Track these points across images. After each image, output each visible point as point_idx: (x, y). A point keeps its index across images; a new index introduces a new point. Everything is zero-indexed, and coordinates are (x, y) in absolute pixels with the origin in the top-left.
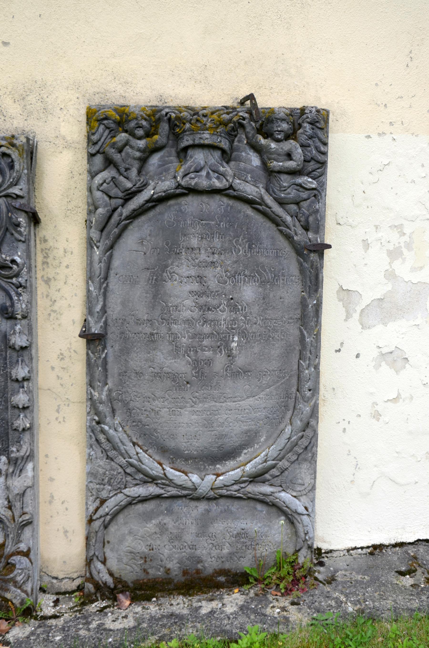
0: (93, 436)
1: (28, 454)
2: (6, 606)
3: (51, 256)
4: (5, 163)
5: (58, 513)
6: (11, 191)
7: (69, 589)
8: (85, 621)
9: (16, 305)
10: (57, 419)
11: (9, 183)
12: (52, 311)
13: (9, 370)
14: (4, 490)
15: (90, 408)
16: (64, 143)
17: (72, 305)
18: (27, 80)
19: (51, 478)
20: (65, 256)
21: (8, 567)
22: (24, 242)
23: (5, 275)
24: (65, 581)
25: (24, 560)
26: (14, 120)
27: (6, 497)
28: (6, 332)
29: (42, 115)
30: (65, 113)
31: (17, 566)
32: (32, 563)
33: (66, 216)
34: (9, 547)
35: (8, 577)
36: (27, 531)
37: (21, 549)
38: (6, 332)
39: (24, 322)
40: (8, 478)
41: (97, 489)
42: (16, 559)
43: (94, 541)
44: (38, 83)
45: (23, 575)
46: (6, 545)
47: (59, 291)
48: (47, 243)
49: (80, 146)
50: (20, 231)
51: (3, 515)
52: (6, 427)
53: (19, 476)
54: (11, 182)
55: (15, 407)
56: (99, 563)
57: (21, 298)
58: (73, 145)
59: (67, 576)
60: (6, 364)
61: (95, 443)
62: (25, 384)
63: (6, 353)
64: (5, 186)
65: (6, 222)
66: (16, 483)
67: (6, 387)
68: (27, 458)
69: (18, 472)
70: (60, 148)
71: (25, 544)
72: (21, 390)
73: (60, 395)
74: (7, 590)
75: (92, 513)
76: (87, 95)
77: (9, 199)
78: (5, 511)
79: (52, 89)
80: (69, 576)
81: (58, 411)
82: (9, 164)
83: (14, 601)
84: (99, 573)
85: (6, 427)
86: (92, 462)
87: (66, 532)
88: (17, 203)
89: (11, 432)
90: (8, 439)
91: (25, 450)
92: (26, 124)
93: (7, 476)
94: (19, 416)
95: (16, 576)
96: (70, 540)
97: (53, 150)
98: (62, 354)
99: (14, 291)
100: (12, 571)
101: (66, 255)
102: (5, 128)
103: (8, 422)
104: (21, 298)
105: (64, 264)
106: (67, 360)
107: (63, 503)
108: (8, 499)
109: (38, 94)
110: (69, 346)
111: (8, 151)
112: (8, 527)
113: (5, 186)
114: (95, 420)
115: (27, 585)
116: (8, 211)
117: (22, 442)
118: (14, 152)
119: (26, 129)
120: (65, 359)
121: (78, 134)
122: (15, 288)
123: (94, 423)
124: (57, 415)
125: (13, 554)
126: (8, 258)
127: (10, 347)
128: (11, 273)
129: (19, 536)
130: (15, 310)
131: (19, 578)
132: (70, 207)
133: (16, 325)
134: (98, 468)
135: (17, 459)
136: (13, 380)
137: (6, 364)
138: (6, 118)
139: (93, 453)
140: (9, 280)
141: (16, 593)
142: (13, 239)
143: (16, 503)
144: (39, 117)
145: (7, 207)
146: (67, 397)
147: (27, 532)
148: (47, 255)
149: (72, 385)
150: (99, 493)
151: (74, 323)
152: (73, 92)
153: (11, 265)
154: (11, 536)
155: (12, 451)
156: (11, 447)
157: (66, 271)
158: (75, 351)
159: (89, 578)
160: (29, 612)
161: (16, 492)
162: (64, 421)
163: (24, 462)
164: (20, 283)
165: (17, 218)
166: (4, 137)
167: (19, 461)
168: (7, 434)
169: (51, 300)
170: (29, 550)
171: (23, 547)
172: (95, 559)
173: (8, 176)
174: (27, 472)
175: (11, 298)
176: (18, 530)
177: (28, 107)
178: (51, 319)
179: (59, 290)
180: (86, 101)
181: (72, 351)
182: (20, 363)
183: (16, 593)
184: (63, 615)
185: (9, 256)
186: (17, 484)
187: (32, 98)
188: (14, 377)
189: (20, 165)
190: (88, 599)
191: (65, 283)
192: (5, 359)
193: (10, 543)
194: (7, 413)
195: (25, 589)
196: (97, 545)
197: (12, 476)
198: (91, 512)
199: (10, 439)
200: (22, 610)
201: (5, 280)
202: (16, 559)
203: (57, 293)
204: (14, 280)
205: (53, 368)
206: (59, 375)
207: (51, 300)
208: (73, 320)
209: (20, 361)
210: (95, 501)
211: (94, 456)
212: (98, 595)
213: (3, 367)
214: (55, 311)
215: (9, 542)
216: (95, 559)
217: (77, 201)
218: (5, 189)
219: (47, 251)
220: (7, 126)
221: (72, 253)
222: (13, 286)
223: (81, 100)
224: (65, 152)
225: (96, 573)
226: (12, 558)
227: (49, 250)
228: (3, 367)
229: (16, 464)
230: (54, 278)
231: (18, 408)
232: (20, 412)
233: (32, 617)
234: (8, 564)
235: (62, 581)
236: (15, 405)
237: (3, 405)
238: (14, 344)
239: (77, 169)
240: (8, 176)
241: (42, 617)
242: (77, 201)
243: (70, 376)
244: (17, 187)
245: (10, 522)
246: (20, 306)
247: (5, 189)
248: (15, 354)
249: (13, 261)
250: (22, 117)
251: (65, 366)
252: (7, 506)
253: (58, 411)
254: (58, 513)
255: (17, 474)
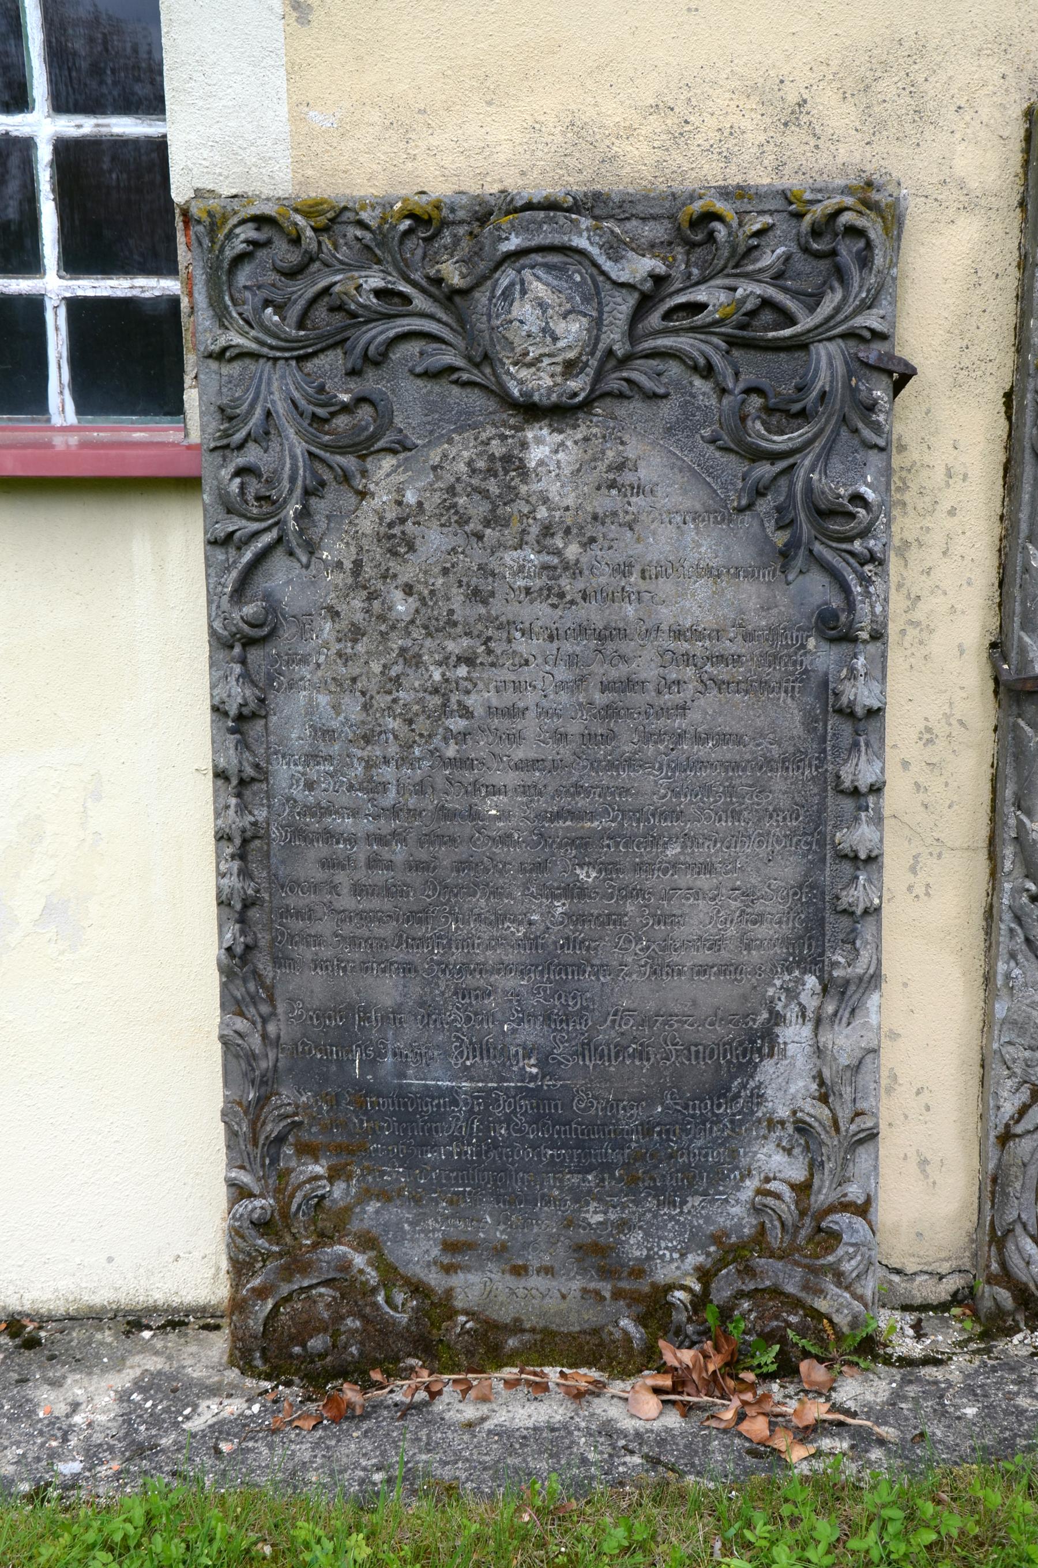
0: (1019, 931)
1: (871, 971)
2: (816, 1328)
3: (914, 487)
4: (850, 251)
5: (906, 1117)
6: (859, 321)
7: (933, 1299)
8: (1014, 1377)
9: (859, 606)
10: (910, 888)
11: (857, 303)
12: (911, 623)
13: (830, 767)
14: (810, 1057)
15: (1013, 863)
16: (962, 198)
17: (959, 607)
18: (878, 39)
19: (891, 1030)
20: (948, 485)
21: (817, 1238)
22: (882, 449)
23: (838, 532)
24: (919, 1279)
25: (859, 1222)
26: (840, 145)
27: (814, 1073)
28: (826, 674)
29: (909, 128)
30: (967, 118)
31: (845, 1238)
32: (874, 1233)
33: (957, 385)
34: (824, 1191)
35: (822, 1261)
36: (864, 1156)
37: (851, 1197)
38: (826, 674)
39: (871, 648)
40: (821, 1029)
41: (1025, 1060)
42: (841, 1220)
43: (1018, 1185)
44: (906, 45)
45: (859, 1258)
46: (815, 1187)
47: (928, 573)
48: (905, 454)
49: (1002, 203)
50: (878, 423)
51: (812, 1116)
52: (820, 905)
53: (849, 1024)
54: (863, 300)
55: (846, 856)
56: (1029, 1240)
57: (872, 589)
58: (983, 202)
59: (925, 1268)
60: (824, 751)
61: (1024, 947)
62: (871, 800)
63: (825, 725)
64: (848, 310)
65: (842, 401)
66: (841, 1041)
67: (822, 808)
68: (869, 982)
69: (847, 1015)
70: (951, 211)
71: (859, 1187)
72: (863, 814)
73: (919, 830)
74: (820, 1292)
75: (1012, 1118)
76: (1029, 66)
77: (852, 343)
78: (813, 1106)
79: (939, 59)
80: (930, 1269)
81: (913, 869)
82: (859, 253)
83: (836, 1319)
84: (1028, 1263)
85: (820, 905)
86: (1012, 995)
87: (924, 1163)
88: (872, 353)
89: (829, 917)
90: (824, 935)
91: (866, 961)
92: (868, 155)
93: (818, 1022)
94: (857, 878)
95: (840, 1260)
96: (934, 1183)
97: (932, 218)
98: (929, 730)
99: (855, 571)
100: (830, 1250)
101: (951, 481)
102: (817, 167)
103: (823, 893)
104: (872, 589)
105: (946, 506)
106: (941, 744)
107: (918, 1093)
108: (819, 1078)
109: (902, 74)
110: (948, 711)
111: (860, 222)
112: (822, 1143)
113: (848, 310)
114: (1028, 890)
115: (863, 1282)
116: (850, 373)
117: (858, 943)
118: (874, 222)
119: (869, 168)
120: (937, 741)
121: (998, 173)
122: (856, 565)
123: (1025, 899)
124: (910, 878)
125: (831, 1209)
126: (842, 491)
127: (839, 711)
128: (853, 528)
129: (845, 1164)
130: (857, 620)
131: (847, 1267)
132: (966, 362)
133: (855, 656)
134: (1029, 1010)
135: (847, 982)
136: (842, 792)
137: (824, 751)
138: (820, 142)
139: (1016, 972)
140: (844, 546)
141: (841, 1300)
142: (856, 442)
143: (843, 1089)
144: (901, 135)
145: (847, 363)
146: (936, 835)
147: (863, 1155)
148: (904, 483)
149: (950, 807)
150: (1029, 1070)
151: (962, 652)
152: (991, 61)
153: (851, 508)
154: (829, 1166)
155: (835, 964)
156: (828, 954)
157: (950, 523)
158: (961, 723)
159: (996, 1276)
160: (870, 1348)
161: (844, 1060)
162: (927, 894)
163: (861, 991)
164: (870, 551)
165: (870, 390)
166: (846, 186)
167: (852, 988)
168: (822, 922)
169: (908, 597)
170: (868, 1201)
171: (854, 1192)
172: (1019, 1229)
173: (856, 285)
174: (868, 1016)
175: (845, 588)
176: (846, 1153)
177: (877, 109)
178: (906, 644)
179: (928, 572)
180: (1024, 82)
181: (954, 722)
182: (863, 749)
183: (841, 1300)
184: (950, 1359)
185: (844, 485)
186: (843, 1041)
187: (888, 87)
188: (847, 784)
189: (885, 257)
190: (993, 1327)
191: (944, 553)
192: (823, 739)
193: (827, 1183)
194: (823, 870)
195: (859, 1291)
196: (1026, 1195)
197: (833, 1022)
198: (1007, 1117)
199: (828, 933)
200: (858, 1339)
201: (834, 545)
202: (841, 1220)
203: (924, 577)
204: (857, 545)
205: (905, 764)
206: (921, 780)
207: (908, 597)
208: (960, 646)
209: (862, 744)
210: (1017, 1090)
211: (1021, 980)
212: (1020, 1317)
213: (817, 758)
214: (915, 624)
215: (822, 1181)
216: (1019, 1229)
217: (985, 345)
218: (847, 319)
219: (904, 474)
220: (822, 163)
221: (965, 477)
222: (852, 560)
223: (1011, 80)
224: (963, 220)
225: (1022, 1265)
226: (830, 1218)
227: (909, 471)
228: (817, 758)
229: (843, 993)
230: (917, 540)
231: (856, 857)
232: (858, 869)
233: (875, 1358)
234: (819, 1230)
235: (914, 1280)
236: (848, 851)
237: (815, 852)
238: (851, 704)
239: (990, 264)
240: (856, 285)
241: (900, 1359)
242: (985, 345)
243: (947, 784)
244: (874, 311)
245: (827, 1132)
246: (867, 608)
247: (847, 319)
248: (847, 729)
249: (858, 499)
250: (859, 136)
251: (934, 761)
252: (817, 1094)
253: (913, 869)
254: (906, 1117)
255: (845, 1020)
